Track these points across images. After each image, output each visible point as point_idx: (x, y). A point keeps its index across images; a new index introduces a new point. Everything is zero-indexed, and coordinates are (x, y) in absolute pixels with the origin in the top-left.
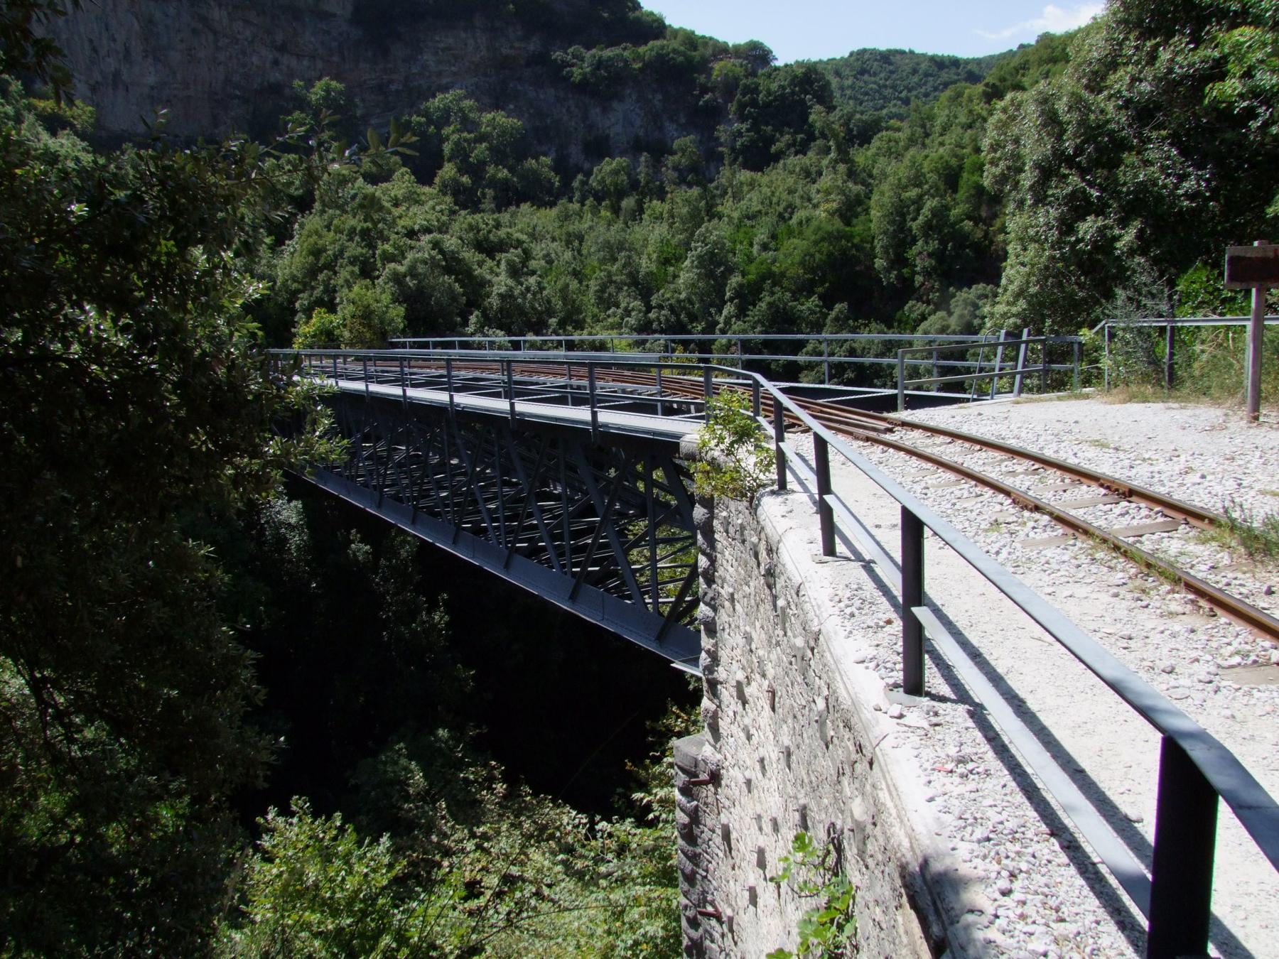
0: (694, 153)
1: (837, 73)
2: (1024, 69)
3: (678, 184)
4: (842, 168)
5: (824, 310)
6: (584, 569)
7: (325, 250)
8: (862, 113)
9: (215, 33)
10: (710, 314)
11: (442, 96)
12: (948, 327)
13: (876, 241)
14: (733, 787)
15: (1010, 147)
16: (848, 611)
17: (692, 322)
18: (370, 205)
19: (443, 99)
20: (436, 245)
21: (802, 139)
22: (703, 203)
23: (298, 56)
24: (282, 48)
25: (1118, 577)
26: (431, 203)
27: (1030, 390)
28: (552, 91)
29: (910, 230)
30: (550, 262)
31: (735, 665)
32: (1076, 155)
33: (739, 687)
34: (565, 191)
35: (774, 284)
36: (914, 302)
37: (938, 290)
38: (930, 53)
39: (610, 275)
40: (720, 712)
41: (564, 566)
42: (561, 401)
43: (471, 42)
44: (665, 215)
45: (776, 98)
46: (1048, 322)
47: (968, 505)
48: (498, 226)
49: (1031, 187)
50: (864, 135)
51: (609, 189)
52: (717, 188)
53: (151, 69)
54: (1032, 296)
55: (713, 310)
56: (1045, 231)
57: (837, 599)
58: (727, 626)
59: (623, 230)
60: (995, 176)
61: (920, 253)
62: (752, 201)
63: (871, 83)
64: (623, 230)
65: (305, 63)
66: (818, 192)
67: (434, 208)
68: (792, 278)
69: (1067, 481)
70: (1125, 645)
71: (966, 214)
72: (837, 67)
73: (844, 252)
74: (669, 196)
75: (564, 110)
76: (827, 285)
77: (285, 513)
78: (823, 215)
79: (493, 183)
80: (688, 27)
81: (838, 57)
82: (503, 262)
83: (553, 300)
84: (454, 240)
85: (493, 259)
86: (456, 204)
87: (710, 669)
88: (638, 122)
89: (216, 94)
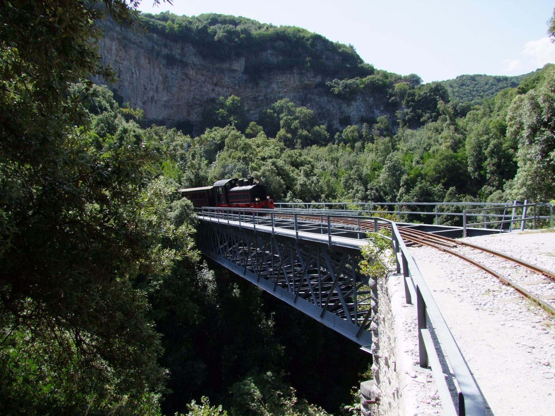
0: (387, 123)
1: (451, 86)
2: (537, 80)
3: (380, 136)
4: (452, 127)
5: (445, 190)
6: (327, 304)
7: (228, 166)
8: (462, 103)
9: (190, 79)
10: (394, 192)
11: (280, 101)
12: (502, 197)
13: (468, 159)
14: (385, 405)
15: (518, 119)
16: (408, 329)
17: (385, 196)
18: (246, 147)
19: (280, 103)
20: (274, 164)
21: (435, 115)
22: (390, 144)
23: (222, 87)
24: (216, 85)
25: (538, 318)
26: (273, 146)
27: (531, 228)
28: (326, 98)
29: (484, 154)
30: (324, 170)
31: (386, 350)
32: (549, 121)
33: (386, 358)
34: (332, 140)
35: (422, 179)
36: (487, 186)
37: (497, 181)
38: (494, 75)
39: (350, 175)
40: (380, 371)
41: (319, 303)
42: (318, 231)
43: (292, 79)
44: (374, 149)
45: (422, 99)
46: (539, 197)
47: (478, 282)
48: (301, 155)
49: (528, 137)
50: (463, 113)
51: (350, 139)
52: (397, 137)
53: (166, 95)
54: (528, 185)
55: (395, 190)
56: (535, 156)
57: (406, 323)
58: (382, 332)
59: (355, 156)
60: (512, 132)
61: (489, 164)
62: (412, 143)
63: (466, 89)
64: (355, 156)
65: (225, 89)
66: (442, 138)
67: (274, 148)
68: (430, 176)
69: (529, 272)
70: (530, 351)
71: (510, 146)
72: (451, 84)
73: (453, 164)
74: (375, 141)
75: (331, 106)
76: (446, 179)
77: (207, 275)
78: (444, 148)
79: (301, 137)
80: (384, 69)
81: (451, 79)
82: (302, 170)
83: (323, 186)
84: (281, 162)
85: (298, 169)
86: (285, 146)
87: (375, 351)
88: (363, 110)
89: (189, 103)
